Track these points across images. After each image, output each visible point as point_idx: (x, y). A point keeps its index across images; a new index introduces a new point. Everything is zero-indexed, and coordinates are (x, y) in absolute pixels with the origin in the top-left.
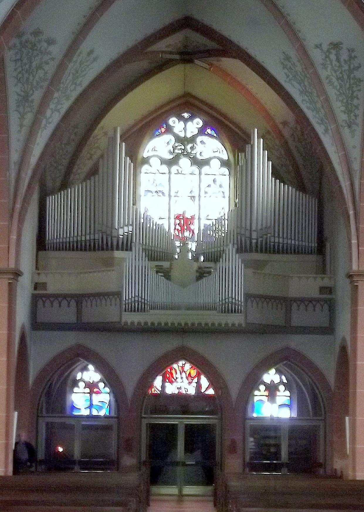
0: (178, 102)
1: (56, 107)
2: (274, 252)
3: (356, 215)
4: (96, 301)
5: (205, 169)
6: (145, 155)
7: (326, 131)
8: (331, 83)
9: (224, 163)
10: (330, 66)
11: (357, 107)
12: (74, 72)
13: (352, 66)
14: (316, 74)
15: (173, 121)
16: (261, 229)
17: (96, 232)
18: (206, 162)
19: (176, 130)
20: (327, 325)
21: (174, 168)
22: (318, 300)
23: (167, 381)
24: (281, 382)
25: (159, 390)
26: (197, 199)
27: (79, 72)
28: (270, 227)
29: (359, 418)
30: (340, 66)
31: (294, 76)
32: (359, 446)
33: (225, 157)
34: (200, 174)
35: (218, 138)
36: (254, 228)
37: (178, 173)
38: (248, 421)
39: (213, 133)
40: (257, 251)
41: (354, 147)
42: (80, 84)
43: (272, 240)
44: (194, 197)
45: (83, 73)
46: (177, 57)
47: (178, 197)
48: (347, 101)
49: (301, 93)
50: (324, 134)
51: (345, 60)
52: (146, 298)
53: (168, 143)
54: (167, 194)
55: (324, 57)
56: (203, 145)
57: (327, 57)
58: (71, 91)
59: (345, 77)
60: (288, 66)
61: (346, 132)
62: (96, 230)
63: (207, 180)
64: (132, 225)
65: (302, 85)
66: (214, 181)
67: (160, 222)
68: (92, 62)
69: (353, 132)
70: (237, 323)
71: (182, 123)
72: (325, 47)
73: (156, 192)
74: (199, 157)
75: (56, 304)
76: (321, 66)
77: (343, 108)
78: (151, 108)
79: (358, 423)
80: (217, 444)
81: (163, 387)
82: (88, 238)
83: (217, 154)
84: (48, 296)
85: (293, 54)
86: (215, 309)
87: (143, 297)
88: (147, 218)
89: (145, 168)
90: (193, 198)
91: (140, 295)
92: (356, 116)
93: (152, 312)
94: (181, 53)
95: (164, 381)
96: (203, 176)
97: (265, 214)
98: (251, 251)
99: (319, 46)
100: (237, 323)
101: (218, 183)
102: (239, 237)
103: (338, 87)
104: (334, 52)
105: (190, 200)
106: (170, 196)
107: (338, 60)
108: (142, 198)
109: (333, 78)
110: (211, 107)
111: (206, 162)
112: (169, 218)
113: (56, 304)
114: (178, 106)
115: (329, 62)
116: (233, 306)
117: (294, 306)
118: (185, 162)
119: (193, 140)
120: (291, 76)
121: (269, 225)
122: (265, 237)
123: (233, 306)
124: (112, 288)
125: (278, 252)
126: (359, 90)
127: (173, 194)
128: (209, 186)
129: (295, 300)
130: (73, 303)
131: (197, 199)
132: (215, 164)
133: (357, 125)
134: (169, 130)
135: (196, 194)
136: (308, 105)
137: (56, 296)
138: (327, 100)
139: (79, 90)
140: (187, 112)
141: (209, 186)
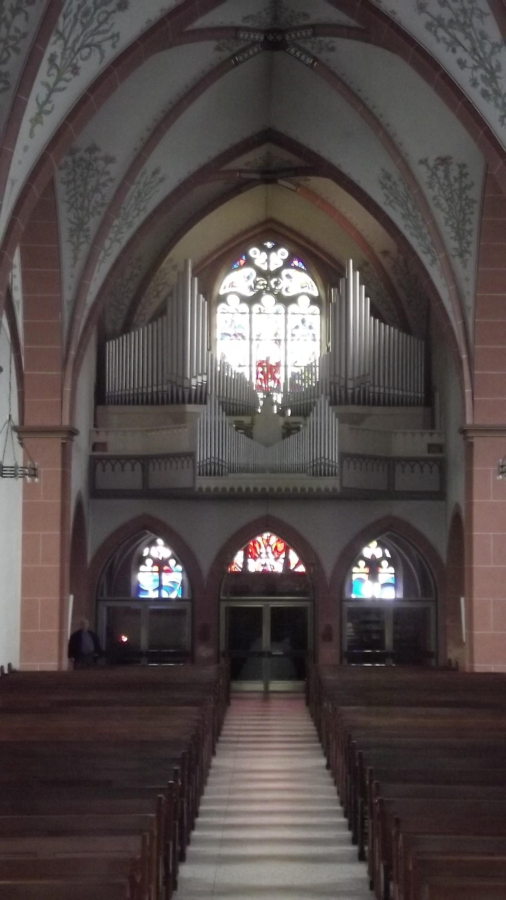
0: (258, 230)
2: (374, 404)
5: (292, 308)
6: (222, 292)
7: (434, 261)
8: (438, 205)
9: (314, 301)
11: (470, 232)
13: (463, 185)
14: (421, 193)
15: (254, 252)
17: (165, 382)
19: (257, 263)
21: (256, 307)
22: (426, 460)
23: (250, 556)
24: (384, 557)
26: (283, 342)
27: (143, 195)
28: (369, 374)
31: (396, 198)
34: (286, 313)
35: (308, 272)
39: (301, 265)
40: (353, 403)
42: (144, 209)
43: (371, 389)
44: (279, 341)
45: (147, 197)
48: (458, 225)
49: (404, 216)
51: (455, 178)
54: (247, 337)
55: (430, 174)
57: (434, 174)
58: (134, 218)
59: (456, 197)
61: (457, 262)
64: (207, 374)
66: (303, 321)
67: (239, 370)
71: (264, 254)
72: (431, 163)
75: (118, 466)
77: (453, 234)
79: (476, 605)
81: (245, 563)
83: (305, 290)
84: (109, 459)
86: (305, 472)
88: (225, 366)
89: (221, 307)
90: (278, 341)
92: (468, 243)
93: (231, 475)
95: (246, 557)
96: (289, 316)
97: (362, 360)
99: (424, 162)
101: (307, 324)
103: (447, 210)
104: (442, 168)
106: (251, 339)
107: (447, 177)
108: (219, 342)
109: (439, 198)
110: (298, 234)
112: (250, 366)
115: (436, 180)
117: (398, 468)
118: (268, 300)
119: (277, 273)
120: (392, 198)
121: (367, 372)
122: (363, 386)
126: (472, 213)
127: (254, 337)
128: (297, 327)
129: (399, 460)
130: (138, 466)
131: (283, 342)
132: (304, 301)
133: (469, 253)
134: (249, 262)
135: (282, 337)
136: (412, 230)
137: (119, 459)
138: (435, 224)
139: (143, 216)
140: (271, 241)
141: (297, 327)
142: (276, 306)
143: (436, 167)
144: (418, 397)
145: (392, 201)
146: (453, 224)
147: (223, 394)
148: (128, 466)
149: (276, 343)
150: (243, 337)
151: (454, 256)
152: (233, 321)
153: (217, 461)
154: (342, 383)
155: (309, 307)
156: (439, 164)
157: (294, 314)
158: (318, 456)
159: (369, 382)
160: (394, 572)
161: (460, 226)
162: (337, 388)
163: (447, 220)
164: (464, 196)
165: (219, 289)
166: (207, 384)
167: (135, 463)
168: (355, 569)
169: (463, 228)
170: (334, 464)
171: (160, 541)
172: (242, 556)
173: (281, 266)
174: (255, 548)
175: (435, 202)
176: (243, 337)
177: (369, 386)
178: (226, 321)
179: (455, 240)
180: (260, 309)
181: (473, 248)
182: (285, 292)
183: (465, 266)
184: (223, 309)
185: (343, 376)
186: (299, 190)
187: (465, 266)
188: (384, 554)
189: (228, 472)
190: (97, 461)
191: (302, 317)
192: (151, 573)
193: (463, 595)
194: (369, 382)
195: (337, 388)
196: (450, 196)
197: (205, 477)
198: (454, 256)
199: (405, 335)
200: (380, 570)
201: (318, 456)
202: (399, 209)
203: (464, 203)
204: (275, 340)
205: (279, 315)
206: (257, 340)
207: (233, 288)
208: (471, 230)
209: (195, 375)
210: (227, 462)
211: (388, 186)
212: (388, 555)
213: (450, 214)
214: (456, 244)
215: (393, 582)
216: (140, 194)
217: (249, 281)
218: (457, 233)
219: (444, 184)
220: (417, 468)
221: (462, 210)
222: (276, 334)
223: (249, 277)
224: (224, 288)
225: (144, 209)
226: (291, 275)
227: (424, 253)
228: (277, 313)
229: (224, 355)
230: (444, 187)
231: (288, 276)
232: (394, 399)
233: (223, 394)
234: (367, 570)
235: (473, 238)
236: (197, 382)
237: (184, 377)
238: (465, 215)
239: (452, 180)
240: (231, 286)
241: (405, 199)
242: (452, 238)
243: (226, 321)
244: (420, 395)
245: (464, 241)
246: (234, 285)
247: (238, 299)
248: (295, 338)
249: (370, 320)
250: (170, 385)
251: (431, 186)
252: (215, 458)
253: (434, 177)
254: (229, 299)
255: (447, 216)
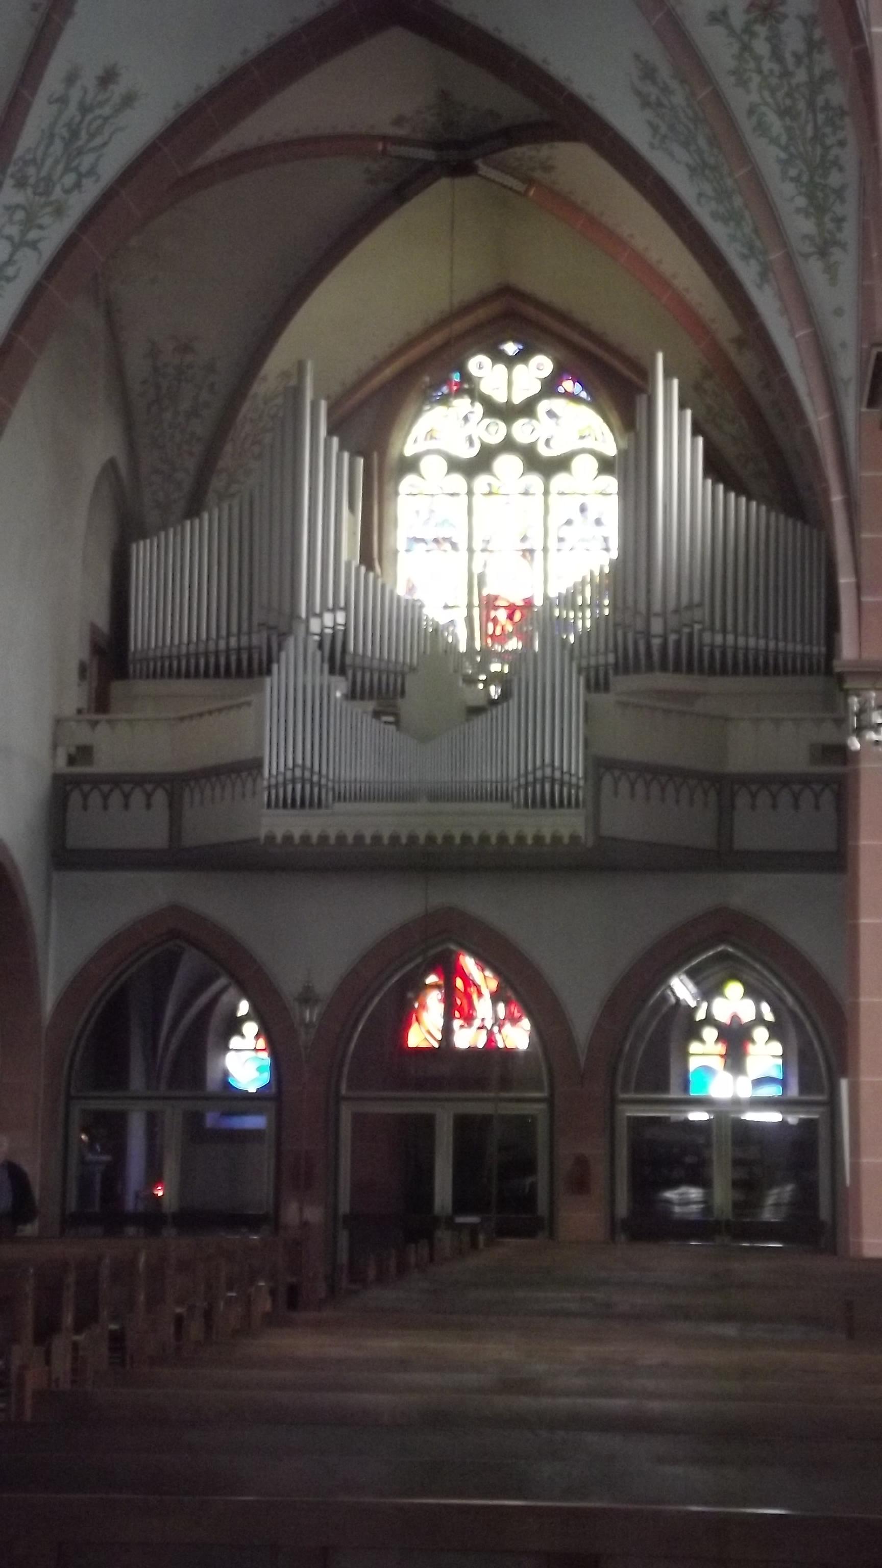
0: (482, 314)
1: (23, 233)
2: (712, 672)
3: (851, 506)
4: (213, 789)
5: (559, 480)
6: (409, 451)
7: (764, 275)
8: (762, 128)
9: (606, 466)
10: (756, 79)
11: (839, 193)
12: (65, 133)
13: (817, 72)
14: (717, 96)
16: (677, 611)
17: (255, 628)
18: (561, 464)
19: (485, 388)
20: (831, 846)
21: (481, 482)
22: (806, 780)
23: (457, 1014)
24: (759, 1020)
25: (435, 1038)
26: (539, 555)
27: (84, 135)
28: (701, 605)
29: (866, 1079)
30: (786, 74)
31: (672, 127)
32: (866, 1160)
33: (610, 449)
34: (546, 493)
35: (595, 404)
36: (657, 607)
37: (490, 493)
38: (620, 1107)
39: (577, 388)
40: (664, 668)
41: (839, 312)
42: (92, 172)
43: (707, 638)
44: (531, 551)
45: (98, 141)
46: (429, 155)
47: (491, 551)
48: (811, 177)
49: (693, 171)
50: (760, 287)
51: (795, 55)
52: (324, 772)
53: (466, 419)
54: (463, 545)
55: (736, 48)
56: (553, 421)
57: (746, 48)
58: (67, 192)
59: (802, 105)
60: (653, 98)
61: (813, 269)
62: (255, 621)
63: (562, 508)
64: (346, 609)
65: (693, 148)
66: (583, 509)
67: (442, 618)
68: (118, 111)
69: (831, 271)
70: (565, 834)
71: (501, 368)
72: (737, 18)
73: (436, 541)
74: (544, 451)
75: (116, 798)
76: (732, 79)
77: (801, 202)
78: (416, 325)
79: (865, 1093)
80: (625, 1188)
81: (447, 1031)
82: (233, 642)
83: (587, 444)
84: (96, 781)
85: (655, 53)
86: (506, 797)
87: (316, 768)
88: (415, 607)
89: (408, 483)
90: (528, 553)
91: (308, 764)
92: (839, 221)
93: (339, 807)
94: (438, 145)
95: (448, 1017)
96: (553, 498)
97: (686, 571)
98: (650, 668)
99: (719, 17)
100: (565, 834)
101: (592, 515)
102: (620, 633)
103: (784, 140)
104: (762, 30)
105: (522, 559)
106: (470, 551)
107: (777, 55)
108: (402, 557)
109: (764, 109)
110: (565, 318)
111: (561, 464)
112: (470, 606)
113: (116, 798)
114: (492, 321)
115: (752, 65)
116: (557, 787)
117: (743, 800)
119: (527, 409)
120: (664, 129)
121: (697, 598)
122: (686, 630)
123: (557, 787)
124: (246, 753)
125: (723, 672)
126: (842, 144)
127: (477, 545)
128: (569, 522)
129: (744, 780)
130: (160, 797)
131: (539, 555)
132: (585, 466)
133: (843, 246)
135: (536, 543)
136: (713, 205)
137: (115, 780)
138: (756, 181)
139: (92, 191)
140: (516, 340)
141: (569, 522)
142: (523, 477)
143: (748, 30)
144: (811, 656)
145: (665, 137)
146: (799, 175)
147: (381, 653)
148: (138, 797)
149: (524, 556)
150: (454, 546)
151: (806, 256)
152: (432, 511)
153: (315, 778)
154: (640, 624)
155: (595, 478)
156: (755, 21)
157: (563, 494)
158: (538, 763)
159: (701, 622)
160: (781, 1053)
161: (817, 179)
162: (630, 636)
163: (786, 164)
164: (820, 100)
165: (404, 443)
166: (345, 632)
167: (154, 790)
168: (694, 1047)
169: (822, 181)
170: (574, 780)
171: (526, 1023)
172: (441, 1015)
173: (537, 393)
174: (469, 997)
175: (754, 119)
176: (454, 546)
177: (701, 631)
178: (417, 512)
179: (807, 215)
180: (489, 485)
181: (849, 233)
182: (545, 447)
183: (833, 280)
184: (412, 486)
185: (642, 607)
186: (532, 193)
187: (833, 280)
188: (759, 1014)
189: (334, 800)
190: (68, 788)
191: (582, 500)
192: (253, 1054)
193: (844, 1073)
194: (701, 622)
195: (630, 636)
196: (788, 102)
197: (281, 811)
198: (806, 256)
199: (790, 522)
200: (751, 1048)
201: (538, 763)
202: (683, 155)
203: (821, 117)
204: (524, 551)
205: (530, 497)
206: (483, 550)
207: (433, 441)
208: (843, 187)
209: (318, 610)
210: (331, 776)
211: (653, 98)
212: (769, 1016)
213: (792, 149)
214: (806, 226)
215: (778, 1074)
216: (75, 134)
217: (468, 425)
218: (811, 197)
219: (771, 71)
220: (785, 797)
221: (818, 137)
222: (524, 539)
223: (467, 417)
224: (415, 441)
225: (92, 172)
226: (556, 410)
227: (745, 257)
228: (526, 493)
229: (413, 586)
230: (774, 81)
231: (551, 414)
232: (756, 660)
233: (381, 653)
234: (721, 1048)
235: (849, 208)
236: (323, 627)
237: (294, 614)
238: (826, 149)
239: (790, 60)
240: (429, 437)
241: (692, 126)
242: (798, 210)
243: (417, 512)
244: (815, 650)
245: (827, 219)
246: (435, 434)
247: (444, 465)
248: (565, 546)
249: (704, 486)
250: (265, 635)
251: (743, 83)
252: (303, 767)
253: (746, 55)
254: (425, 464)
255: (783, 155)
